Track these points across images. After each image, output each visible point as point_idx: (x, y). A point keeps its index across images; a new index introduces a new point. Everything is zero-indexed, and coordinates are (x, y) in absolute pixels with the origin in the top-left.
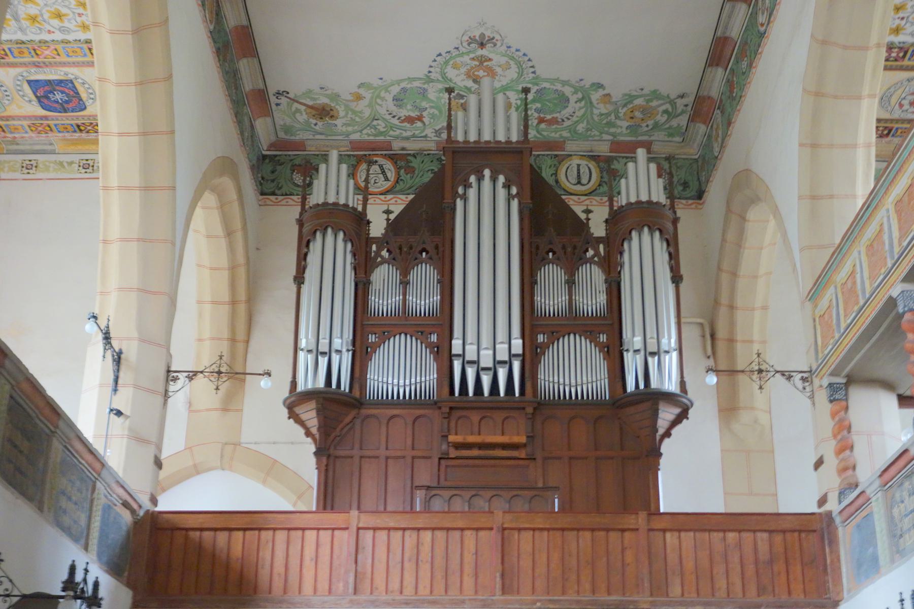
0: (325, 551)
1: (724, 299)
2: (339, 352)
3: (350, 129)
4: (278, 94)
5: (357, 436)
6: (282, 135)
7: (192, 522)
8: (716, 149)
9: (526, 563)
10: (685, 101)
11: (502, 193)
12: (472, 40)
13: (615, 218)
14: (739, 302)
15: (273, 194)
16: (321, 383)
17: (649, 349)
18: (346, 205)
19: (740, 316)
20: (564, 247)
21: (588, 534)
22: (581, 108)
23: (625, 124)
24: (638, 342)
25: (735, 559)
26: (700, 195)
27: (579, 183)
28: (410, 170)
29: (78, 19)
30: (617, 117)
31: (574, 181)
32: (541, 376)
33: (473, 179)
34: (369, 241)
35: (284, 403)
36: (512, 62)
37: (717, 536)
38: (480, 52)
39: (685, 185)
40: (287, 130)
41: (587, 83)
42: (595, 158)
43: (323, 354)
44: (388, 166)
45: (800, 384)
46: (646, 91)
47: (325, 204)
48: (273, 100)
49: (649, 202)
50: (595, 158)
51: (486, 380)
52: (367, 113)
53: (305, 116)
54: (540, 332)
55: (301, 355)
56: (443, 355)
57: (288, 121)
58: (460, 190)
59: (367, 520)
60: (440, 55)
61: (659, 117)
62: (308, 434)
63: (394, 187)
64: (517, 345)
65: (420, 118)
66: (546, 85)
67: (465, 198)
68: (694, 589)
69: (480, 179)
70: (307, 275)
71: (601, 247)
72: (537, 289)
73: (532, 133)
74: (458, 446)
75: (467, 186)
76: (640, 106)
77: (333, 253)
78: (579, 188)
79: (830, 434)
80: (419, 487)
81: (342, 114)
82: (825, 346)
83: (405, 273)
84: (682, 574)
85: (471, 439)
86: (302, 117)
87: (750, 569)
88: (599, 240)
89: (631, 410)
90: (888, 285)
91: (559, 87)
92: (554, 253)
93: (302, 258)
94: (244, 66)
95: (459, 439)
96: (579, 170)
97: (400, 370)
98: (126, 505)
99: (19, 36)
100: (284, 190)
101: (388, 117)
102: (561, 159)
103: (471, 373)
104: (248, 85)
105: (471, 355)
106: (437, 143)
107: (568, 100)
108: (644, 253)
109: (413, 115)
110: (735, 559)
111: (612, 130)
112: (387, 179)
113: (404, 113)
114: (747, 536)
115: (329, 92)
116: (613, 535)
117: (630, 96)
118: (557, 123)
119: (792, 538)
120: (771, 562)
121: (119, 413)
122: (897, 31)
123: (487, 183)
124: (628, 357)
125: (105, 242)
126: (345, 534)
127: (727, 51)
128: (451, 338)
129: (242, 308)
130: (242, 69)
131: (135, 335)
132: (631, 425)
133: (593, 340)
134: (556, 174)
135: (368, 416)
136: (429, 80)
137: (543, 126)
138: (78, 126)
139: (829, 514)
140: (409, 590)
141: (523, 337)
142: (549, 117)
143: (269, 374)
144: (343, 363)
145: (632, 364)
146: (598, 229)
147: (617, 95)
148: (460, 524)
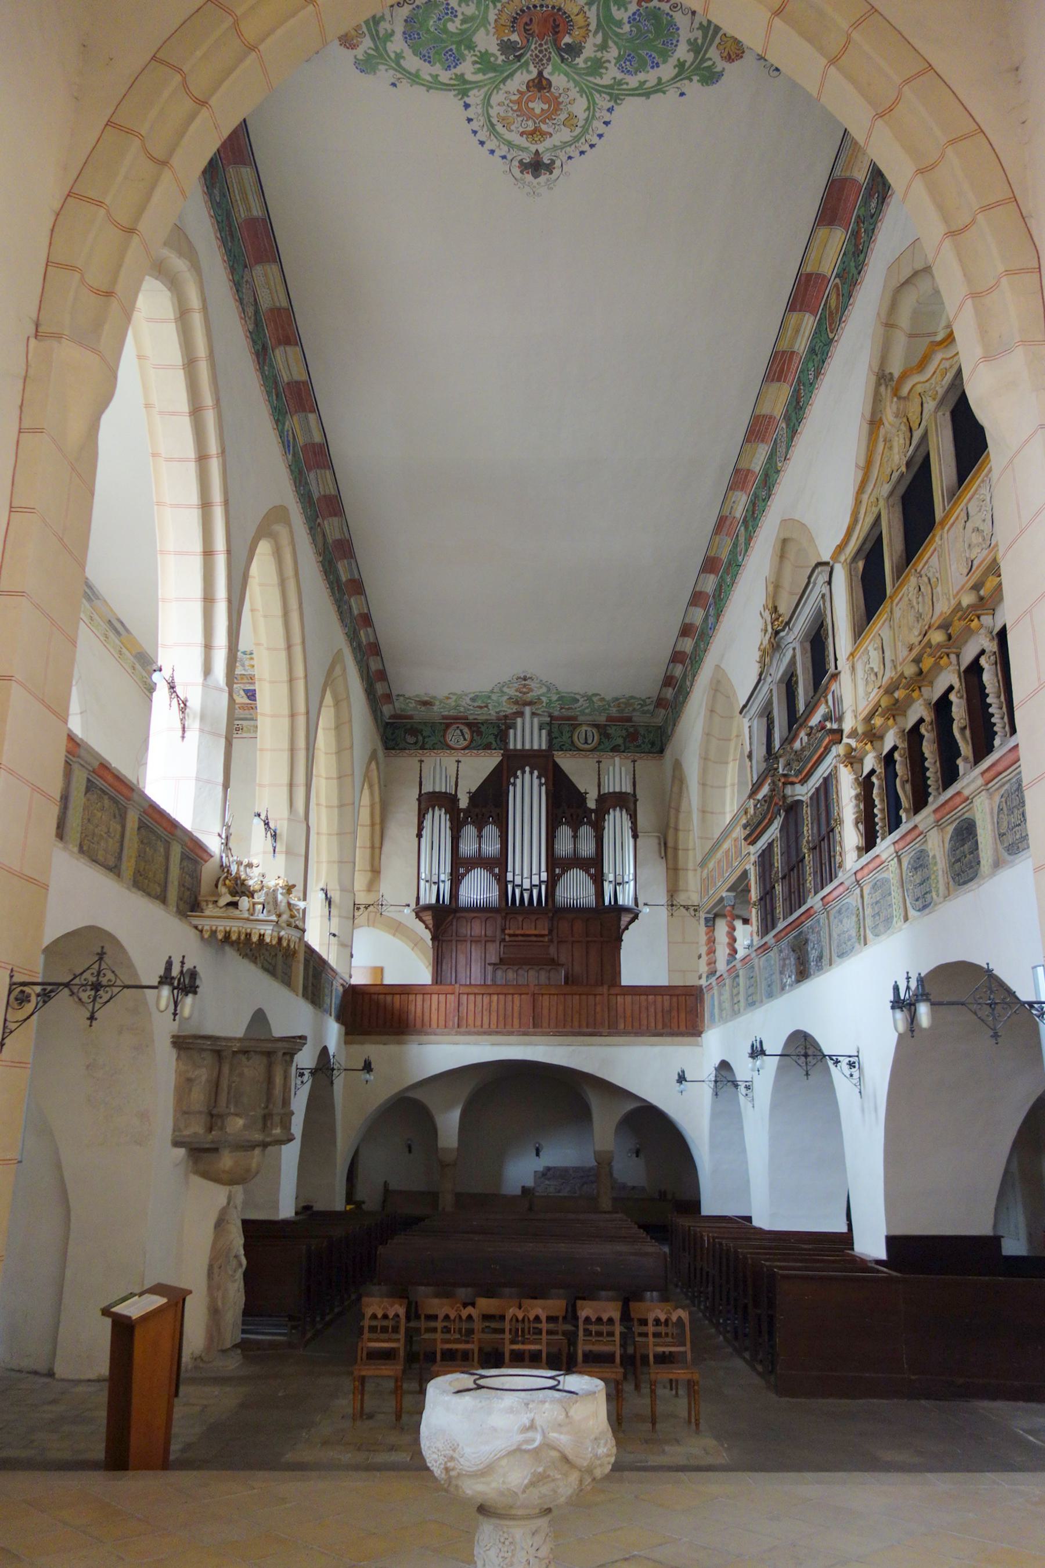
0: (442, 1005)
1: (672, 825)
2: (443, 881)
4: (398, 695)
5: (454, 927)
8: (688, 683)
9: (545, 1012)
11: (536, 782)
13: (602, 799)
14: (681, 827)
15: (393, 749)
16: (434, 901)
19: (681, 835)
21: (578, 997)
23: (614, 710)
24: (611, 877)
25: (652, 1010)
27: (586, 743)
28: (480, 733)
31: (583, 741)
34: (460, 810)
37: (643, 998)
39: (653, 744)
41: (590, 694)
42: (597, 726)
44: (466, 730)
45: (693, 913)
48: (394, 698)
49: (621, 793)
50: (597, 726)
51: (526, 895)
52: (453, 704)
54: (557, 866)
55: (422, 883)
56: (502, 881)
57: (403, 706)
58: (512, 780)
62: (427, 927)
64: (544, 876)
65: (487, 706)
67: (514, 785)
69: (524, 772)
70: (424, 833)
72: (556, 842)
74: (510, 935)
77: (438, 821)
84: (625, 1017)
85: (518, 932)
87: (660, 1015)
88: (592, 811)
93: (420, 828)
95: (511, 932)
97: (477, 889)
99: (243, 672)
100: (400, 746)
102: (575, 727)
105: (518, 881)
108: (616, 822)
110: (652, 1010)
113: (476, 704)
114: (659, 998)
116: (591, 998)
119: (682, 999)
120: (670, 1011)
121: (334, 935)
123: (527, 776)
124: (606, 884)
126: (452, 997)
129: (378, 827)
131: (338, 887)
132: (608, 923)
133: (587, 872)
134: (571, 737)
136: (492, 692)
139: (701, 986)
140: (486, 1026)
141: (547, 871)
144: (446, 887)
145: (608, 889)
146: (591, 804)
148: (511, 991)
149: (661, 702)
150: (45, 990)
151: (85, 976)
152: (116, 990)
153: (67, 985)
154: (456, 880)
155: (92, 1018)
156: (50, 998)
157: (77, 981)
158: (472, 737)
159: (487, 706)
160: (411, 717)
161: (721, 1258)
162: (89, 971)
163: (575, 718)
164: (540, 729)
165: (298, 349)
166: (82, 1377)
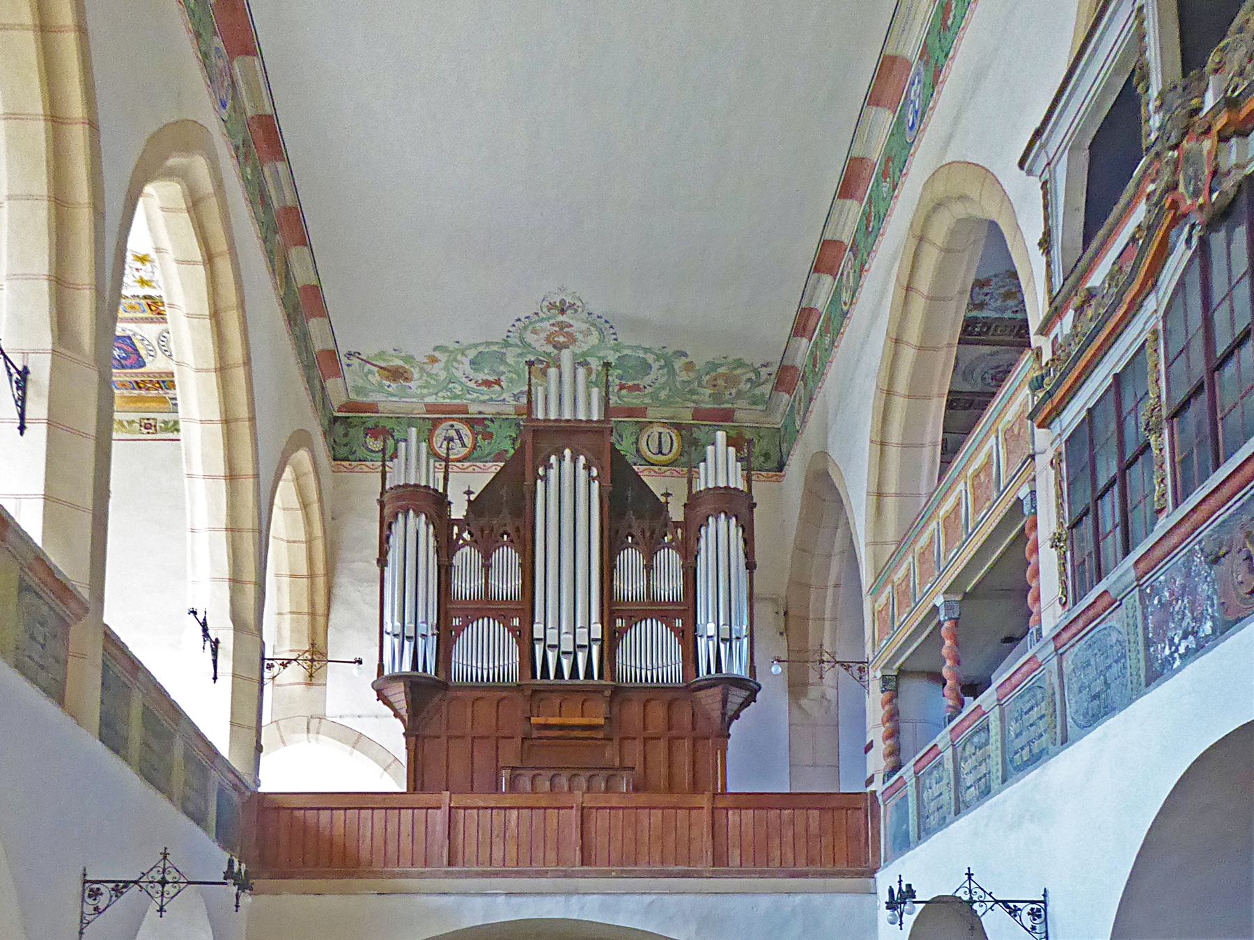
2: (423, 636)
3: (425, 391)
4: (349, 355)
6: (353, 396)
7: (296, 803)
8: (798, 423)
10: (768, 370)
11: (582, 474)
12: (552, 306)
13: (692, 502)
16: (407, 667)
17: (721, 636)
18: (427, 487)
20: (643, 532)
22: (663, 375)
23: (709, 391)
26: (781, 467)
27: (660, 452)
28: (488, 436)
29: (137, 275)
30: (700, 385)
31: (655, 450)
32: (619, 660)
33: (553, 459)
35: (373, 685)
36: (593, 329)
37: (773, 813)
38: (561, 318)
39: (767, 456)
40: (359, 390)
42: (678, 427)
43: (409, 638)
44: (465, 431)
45: (857, 675)
46: (730, 360)
47: (406, 485)
48: (344, 360)
50: (678, 427)
53: (378, 377)
54: (617, 614)
56: (526, 640)
57: (360, 383)
58: (541, 471)
59: (458, 800)
60: (519, 320)
61: (742, 386)
63: (471, 453)
65: (498, 382)
66: (626, 352)
67: (545, 479)
68: (751, 859)
69: (561, 460)
70: (390, 557)
71: (679, 531)
73: (613, 400)
75: (548, 467)
76: (724, 374)
77: (415, 529)
78: (660, 458)
79: (880, 722)
80: (504, 768)
81: (416, 376)
82: (881, 640)
83: (487, 556)
85: (552, 721)
86: (375, 378)
87: (801, 843)
89: (701, 694)
90: (1017, 486)
91: (641, 354)
92: (633, 537)
93: (384, 541)
94: (315, 325)
95: (541, 720)
96: (660, 438)
97: (485, 653)
98: (235, 787)
101: (464, 380)
102: (642, 426)
103: (552, 656)
104: (318, 345)
105: (552, 640)
106: (516, 407)
107: (650, 367)
109: (491, 379)
111: (694, 397)
112: (464, 445)
113: (481, 376)
115: (403, 354)
117: (713, 363)
118: (639, 390)
122: (981, 306)
124: (702, 643)
125: (193, 531)
127: (811, 323)
128: (533, 622)
129: (321, 582)
130: (312, 330)
134: (638, 451)
135: (454, 698)
136: (506, 344)
137: (624, 392)
138: (137, 383)
142: (630, 383)
143: (360, 662)
146: (676, 513)
147: (699, 364)
149: (785, 377)
151: (151, 874)
153: (136, 882)
154: (446, 639)
155: (161, 910)
158: (475, 439)
159: (498, 382)
160: (372, 408)
163: (642, 411)
164: (588, 387)
165: (326, 321)
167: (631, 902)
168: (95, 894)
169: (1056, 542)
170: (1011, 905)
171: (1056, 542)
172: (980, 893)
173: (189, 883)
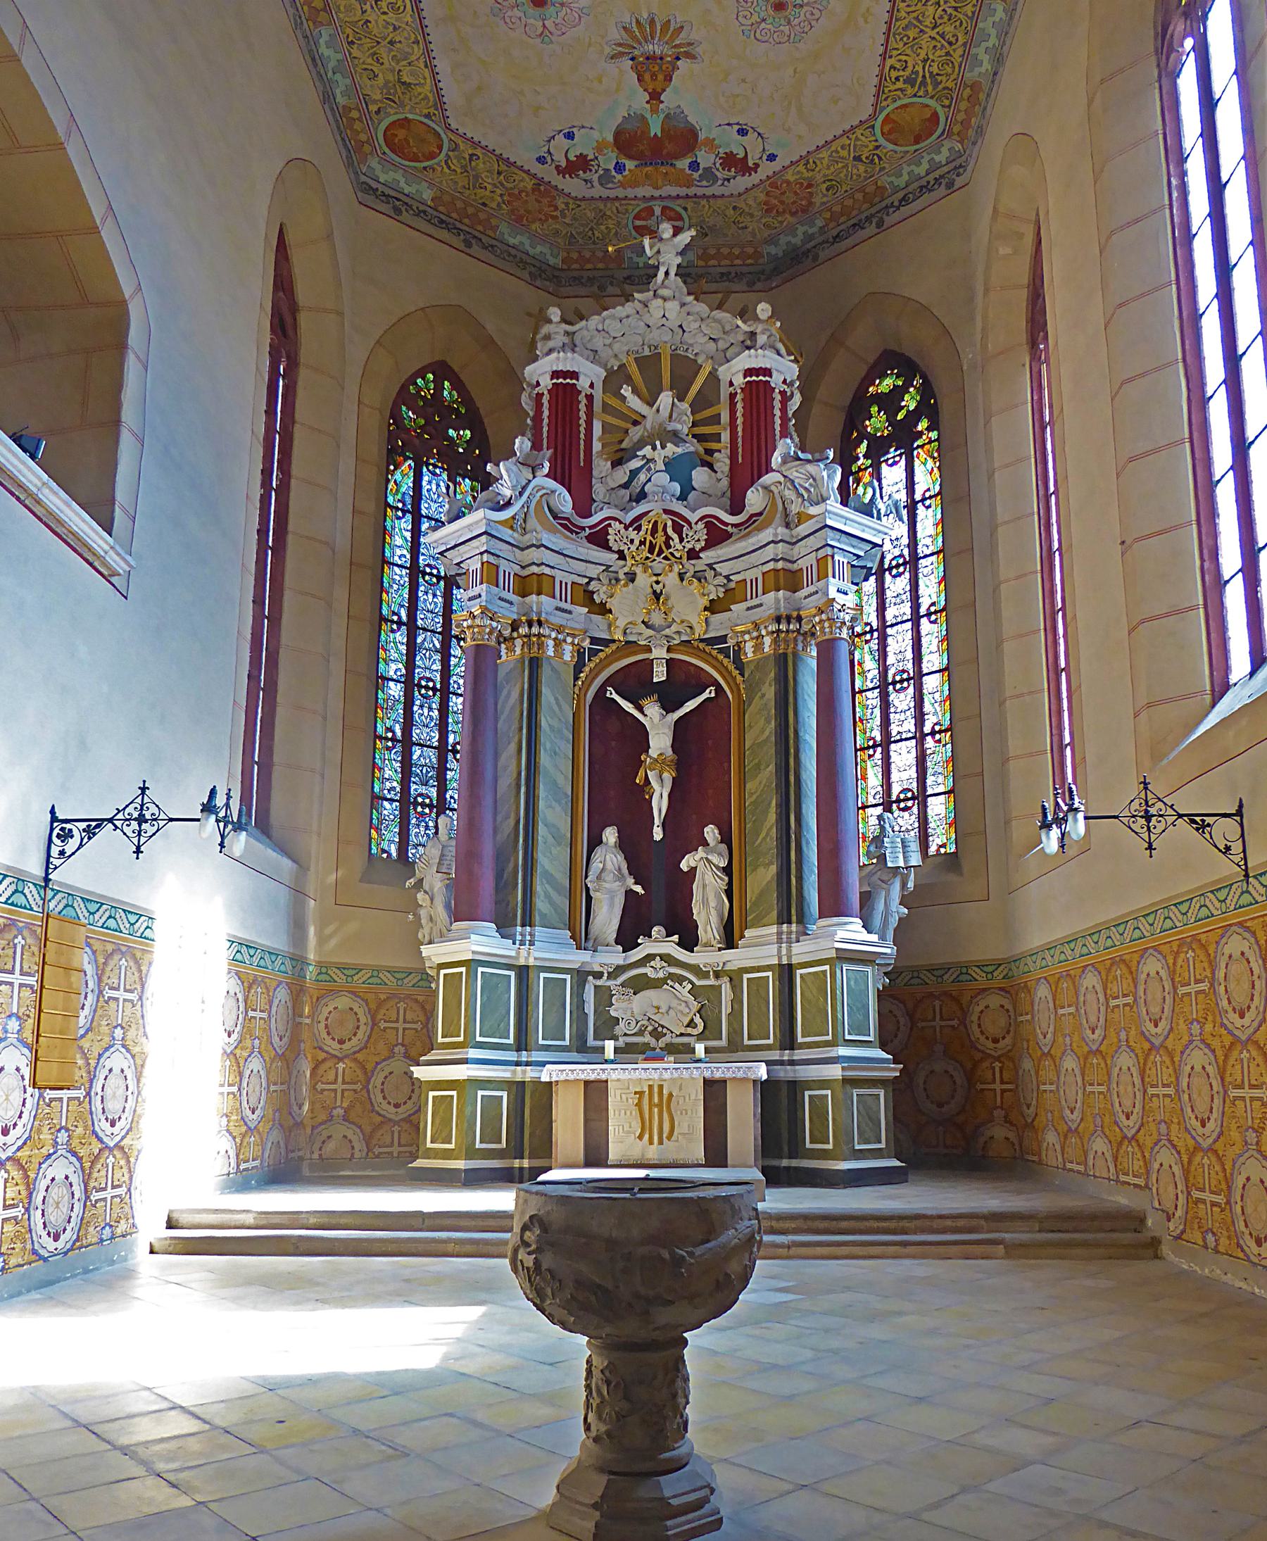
150: (89, 826)
151: (127, 811)
152: (162, 823)
153: (111, 820)
155: (143, 789)
156: (94, 834)
157: (120, 816)
161: (792, 1063)
162: (149, 834)
166: (150, 1438)
167: (808, 765)
168: (66, 836)
169: (600, 439)
170: (1198, 819)
171: (600, 439)
172: (127, 830)
173: (171, 820)
